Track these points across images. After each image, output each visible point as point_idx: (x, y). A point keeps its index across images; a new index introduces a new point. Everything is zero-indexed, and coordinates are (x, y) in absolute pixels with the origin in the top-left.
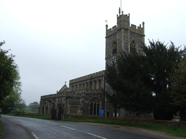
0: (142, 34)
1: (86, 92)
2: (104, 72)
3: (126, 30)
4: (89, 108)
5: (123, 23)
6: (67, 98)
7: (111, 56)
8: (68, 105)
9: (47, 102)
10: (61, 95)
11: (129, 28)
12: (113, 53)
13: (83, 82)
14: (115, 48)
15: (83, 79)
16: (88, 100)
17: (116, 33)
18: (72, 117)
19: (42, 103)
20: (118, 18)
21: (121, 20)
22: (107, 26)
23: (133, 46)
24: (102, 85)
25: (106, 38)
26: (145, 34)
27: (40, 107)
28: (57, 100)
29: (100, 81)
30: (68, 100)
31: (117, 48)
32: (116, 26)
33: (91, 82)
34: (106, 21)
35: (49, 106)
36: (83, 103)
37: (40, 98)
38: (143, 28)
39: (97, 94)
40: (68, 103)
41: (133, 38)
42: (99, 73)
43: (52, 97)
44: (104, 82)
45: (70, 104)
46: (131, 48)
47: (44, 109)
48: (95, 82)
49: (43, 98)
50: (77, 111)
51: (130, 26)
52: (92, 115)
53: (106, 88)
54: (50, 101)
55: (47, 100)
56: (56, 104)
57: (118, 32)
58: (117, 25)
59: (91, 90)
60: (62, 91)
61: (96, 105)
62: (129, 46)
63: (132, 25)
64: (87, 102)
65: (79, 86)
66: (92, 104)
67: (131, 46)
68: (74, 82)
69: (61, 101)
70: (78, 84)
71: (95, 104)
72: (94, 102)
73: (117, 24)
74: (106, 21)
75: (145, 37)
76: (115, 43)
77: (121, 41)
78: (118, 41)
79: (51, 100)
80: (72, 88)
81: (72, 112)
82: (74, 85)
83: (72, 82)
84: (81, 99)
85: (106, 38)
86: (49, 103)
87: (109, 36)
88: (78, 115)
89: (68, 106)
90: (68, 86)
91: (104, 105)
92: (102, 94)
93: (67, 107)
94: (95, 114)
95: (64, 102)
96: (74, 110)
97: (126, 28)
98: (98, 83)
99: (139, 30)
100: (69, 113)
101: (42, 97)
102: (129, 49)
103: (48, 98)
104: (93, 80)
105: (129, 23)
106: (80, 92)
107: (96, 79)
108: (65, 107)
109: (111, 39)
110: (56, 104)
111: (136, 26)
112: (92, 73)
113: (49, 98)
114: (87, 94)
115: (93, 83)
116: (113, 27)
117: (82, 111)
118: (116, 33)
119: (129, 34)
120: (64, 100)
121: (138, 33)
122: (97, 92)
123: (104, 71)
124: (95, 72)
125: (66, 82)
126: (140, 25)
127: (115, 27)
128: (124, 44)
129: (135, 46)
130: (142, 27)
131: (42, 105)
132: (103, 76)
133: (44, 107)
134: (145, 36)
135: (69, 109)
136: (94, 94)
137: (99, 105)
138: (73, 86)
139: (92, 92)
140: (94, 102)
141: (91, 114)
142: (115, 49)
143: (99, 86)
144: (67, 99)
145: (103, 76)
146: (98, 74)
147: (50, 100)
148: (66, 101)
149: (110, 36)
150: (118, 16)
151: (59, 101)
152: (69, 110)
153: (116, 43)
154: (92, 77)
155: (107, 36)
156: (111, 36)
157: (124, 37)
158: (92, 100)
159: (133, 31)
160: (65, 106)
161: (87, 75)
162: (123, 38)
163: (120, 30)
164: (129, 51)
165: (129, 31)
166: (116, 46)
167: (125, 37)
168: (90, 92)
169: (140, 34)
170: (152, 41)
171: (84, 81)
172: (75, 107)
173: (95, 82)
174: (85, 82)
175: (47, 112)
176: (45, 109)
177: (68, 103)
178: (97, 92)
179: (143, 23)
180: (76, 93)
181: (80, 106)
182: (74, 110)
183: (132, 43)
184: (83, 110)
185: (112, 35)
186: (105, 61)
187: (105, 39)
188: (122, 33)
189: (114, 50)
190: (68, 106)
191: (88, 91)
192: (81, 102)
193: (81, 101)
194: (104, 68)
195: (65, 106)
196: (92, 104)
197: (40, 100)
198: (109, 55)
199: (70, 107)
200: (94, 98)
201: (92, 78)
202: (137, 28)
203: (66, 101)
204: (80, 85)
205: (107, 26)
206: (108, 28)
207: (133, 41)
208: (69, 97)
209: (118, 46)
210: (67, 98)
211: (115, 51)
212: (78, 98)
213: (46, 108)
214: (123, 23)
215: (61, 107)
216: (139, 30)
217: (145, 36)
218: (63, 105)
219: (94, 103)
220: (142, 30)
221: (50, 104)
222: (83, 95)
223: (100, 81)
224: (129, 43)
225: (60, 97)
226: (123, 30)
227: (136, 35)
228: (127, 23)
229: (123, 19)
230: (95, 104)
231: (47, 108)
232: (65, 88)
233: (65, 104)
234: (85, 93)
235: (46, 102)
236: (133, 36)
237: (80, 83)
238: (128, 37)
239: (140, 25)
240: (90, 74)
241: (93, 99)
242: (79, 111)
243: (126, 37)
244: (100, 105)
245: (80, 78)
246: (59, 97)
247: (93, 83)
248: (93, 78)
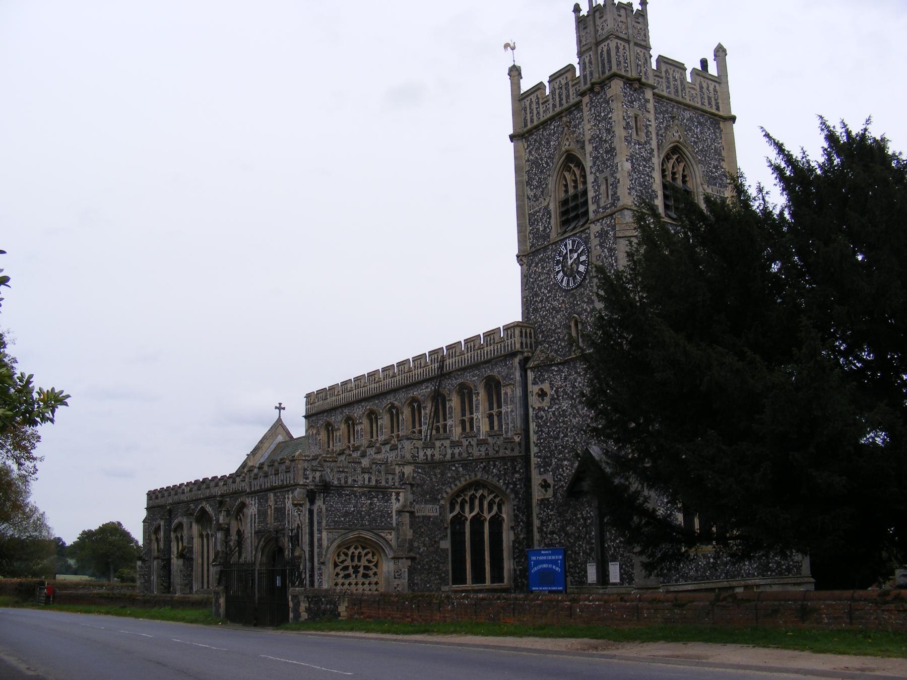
0: (718, 109)
1: (421, 454)
2: (517, 332)
3: (636, 85)
4: (446, 544)
5: (617, 48)
6: (311, 496)
7: (554, 236)
8: (324, 534)
9: (185, 520)
10: (275, 481)
11: (650, 74)
12: (565, 223)
13: (391, 399)
14: (571, 191)
15: (389, 383)
16: (434, 500)
17: (578, 106)
18: (357, 602)
19: (157, 530)
20: (581, 22)
21: (602, 34)
22: (515, 73)
23: (674, 179)
24: (511, 410)
25: (512, 138)
26: (734, 112)
27: (150, 551)
28: (252, 509)
29: (493, 387)
30: (319, 503)
31: (585, 193)
32: (570, 68)
33: (439, 399)
34: (513, 49)
35: (196, 542)
36: (406, 518)
37: (143, 502)
38: (721, 80)
39: (488, 459)
40: (319, 523)
41: (675, 135)
42: (357, 387)
43: (218, 491)
44: (519, 392)
45: (334, 526)
46: (665, 187)
47: (169, 560)
48: (466, 392)
49: (161, 501)
50: (376, 566)
51: (654, 67)
52: (464, 581)
53: (533, 426)
54: (203, 518)
55: (189, 514)
56: (248, 530)
57: (586, 99)
58: (575, 61)
59: (447, 443)
60: (262, 458)
61: (482, 523)
62: (657, 175)
63: (661, 60)
64: (430, 510)
65: (366, 422)
66: (458, 521)
67: (664, 176)
68: (331, 401)
69: (280, 512)
70: (358, 412)
71: (477, 521)
72: (471, 510)
73: (580, 54)
74: (506, 46)
75: (737, 128)
76: (571, 160)
77: (611, 151)
78: (589, 148)
79: (209, 509)
80: (323, 435)
81: (347, 576)
82: (337, 419)
83: (320, 405)
84: (398, 494)
85: (512, 138)
86: (195, 528)
87: (529, 126)
88: (382, 589)
89: (325, 543)
90: (298, 429)
91: (529, 524)
92: (513, 459)
93: (320, 546)
94: (479, 577)
95: (297, 518)
96: (356, 562)
97: (634, 75)
98: (481, 398)
99: (701, 87)
100: (332, 583)
101: (152, 495)
102: (660, 193)
103: (188, 502)
104: (450, 385)
105: (647, 48)
106: (386, 454)
107: (470, 378)
108: (307, 548)
109: (548, 143)
110: (248, 530)
111: (681, 67)
112: (443, 343)
113: (197, 501)
114: (431, 464)
115: (454, 402)
116: (553, 79)
117: (405, 565)
118: (578, 106)
119: (650, 106)
120: (295, 505)
121: (699, 105)
122: (483, 449)
123: (516, 325)
124: (460, 336)
125: (280, 408)
126: (704, 63)
127: (569, 75)
128: (628, 166)
129: (684, 176)
130: (713, 70)
131: (158, 540)
132: (513, 354)
133: (168, 550)
134: (733, 119)
135: (330, 557)
136: (468, 464)
137: (496, 522)
138: (329, 428)
139: (457, 451)
140: (471, 510)
141: (459, 578)
142: (575, 197)
143: (490, 417)
144: (312, 502)
145: (513, 354)
146: (481, 347)
147: (203, 510)
148: (311, 512)
149: (537, 128)
150: (584, 11)
151: (262, 514)
152: (331, 566)
153: (580, 165)
154: (441, 367)
155: (521, 131)
156: (544, 124)
157: (627, 127)
158: (458, 496)
159: (672, 96)
160: (306, 539)
161: (409, 354)
162: (620, 132)
163: (597, 89)
164: (659, 202)
165: (649, 94)
166: (579, 180)
167: (633, 124)
168: (441, 450)
169: (707, 108)
170: (834, 123)
171: (394, 391)
172: (363, 543)
173: (466, 392)
174: (402, 396)
175: (190, 575)
176: (176, 563)
177: (319, 523)
178: (483, 449)
179: (720, 52)
180: (365, 462)
181: (391, 537)
182: (356, 562)
183: (668, 157)
184: (413, 559)
185: (552, 119)
186: (516, 271)
187: (511, 145)
188: (613, 105)
189: (565, 202)
190: (320, 539)
191: (433, 447)
192: (399, 512)
193: (395, 506)
194: (516, 316)
195: (306, 539)
196: (458, 521)
197: (144, 514)
198: (536, 235)
199: (335, 544)
200: (469, 486)
201: (442, 374)
202: (689, 79)
203: (311, 512)
204: (372, 416)
205: (515, 73)
206: (526, 85)
207: (675, 150)
208: (325, 488)
209: (590, 179)
210: (311, 496)
211: (576, 207)
212: (382, 492)
213: (181, 555)
214: (617, 48)
215: (281, 550)
216: (701, 87)
217: (733, 119)
218: (295, 540)
219: (469, 516)
220: (715, 90)
221: (201, 536)
222: (408, 470)
223: (493, 387)
224: (656, 161)
225: (272, 489)
226: (616, 87)
227: (687, 114)
228: (638, 50)
229: (55, 400)
230: (477, 521)
231: (186, 556)
232: (280, 438)
233: (306, 529)
234: (414, 462)
235: (180, 526)
236: (673, 118)
237: (369, 406)
238: (647, 126)
239: (704, 63)
240: (432, 353)
241: (463, 490)
242: (387, 567)
243: (635, 124)
244: (505, 526)
245: (332, 388)
246: (261, 494)
247: (454, 402)
248: (450, 373)
